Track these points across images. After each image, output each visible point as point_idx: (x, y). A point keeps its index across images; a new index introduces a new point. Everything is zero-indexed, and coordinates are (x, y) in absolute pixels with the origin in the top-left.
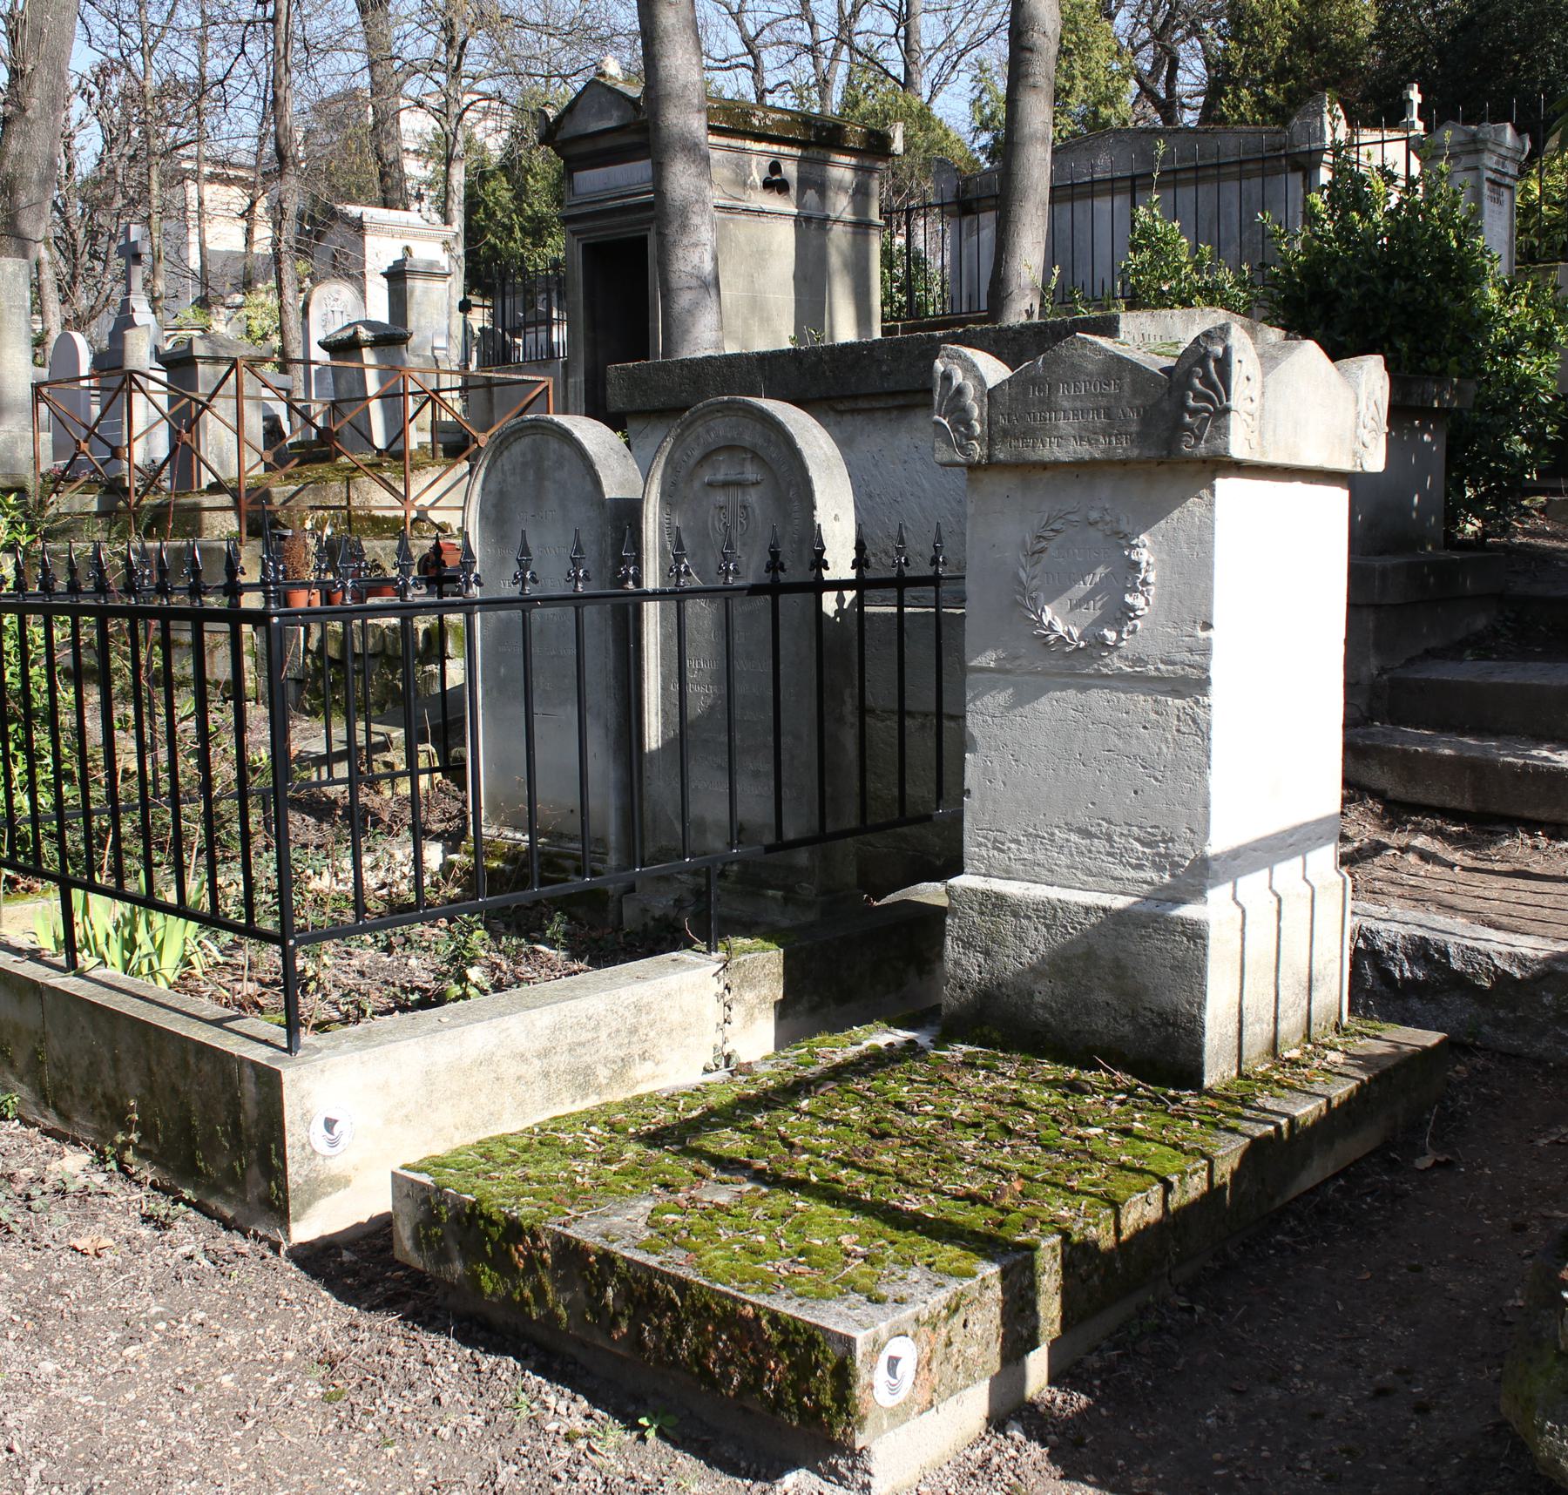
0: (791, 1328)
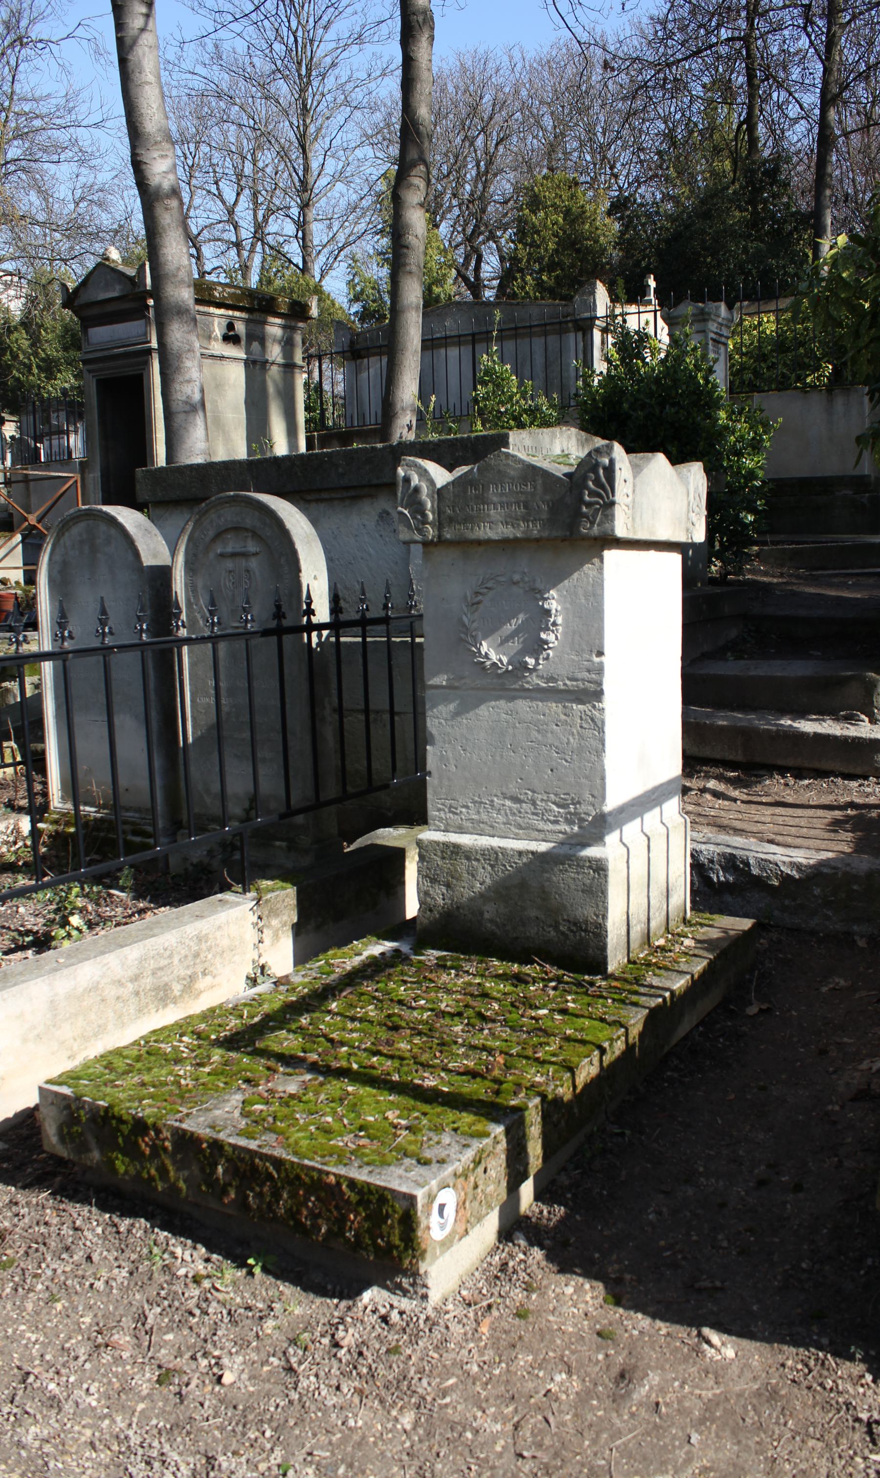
0: (366, 1190)
